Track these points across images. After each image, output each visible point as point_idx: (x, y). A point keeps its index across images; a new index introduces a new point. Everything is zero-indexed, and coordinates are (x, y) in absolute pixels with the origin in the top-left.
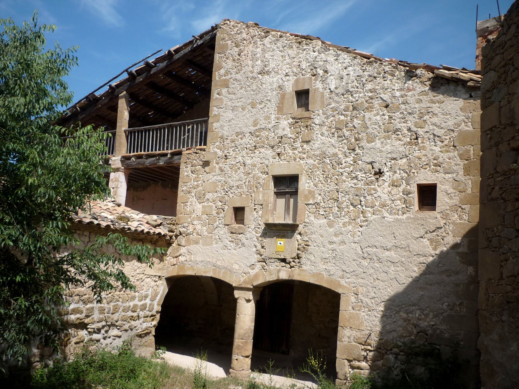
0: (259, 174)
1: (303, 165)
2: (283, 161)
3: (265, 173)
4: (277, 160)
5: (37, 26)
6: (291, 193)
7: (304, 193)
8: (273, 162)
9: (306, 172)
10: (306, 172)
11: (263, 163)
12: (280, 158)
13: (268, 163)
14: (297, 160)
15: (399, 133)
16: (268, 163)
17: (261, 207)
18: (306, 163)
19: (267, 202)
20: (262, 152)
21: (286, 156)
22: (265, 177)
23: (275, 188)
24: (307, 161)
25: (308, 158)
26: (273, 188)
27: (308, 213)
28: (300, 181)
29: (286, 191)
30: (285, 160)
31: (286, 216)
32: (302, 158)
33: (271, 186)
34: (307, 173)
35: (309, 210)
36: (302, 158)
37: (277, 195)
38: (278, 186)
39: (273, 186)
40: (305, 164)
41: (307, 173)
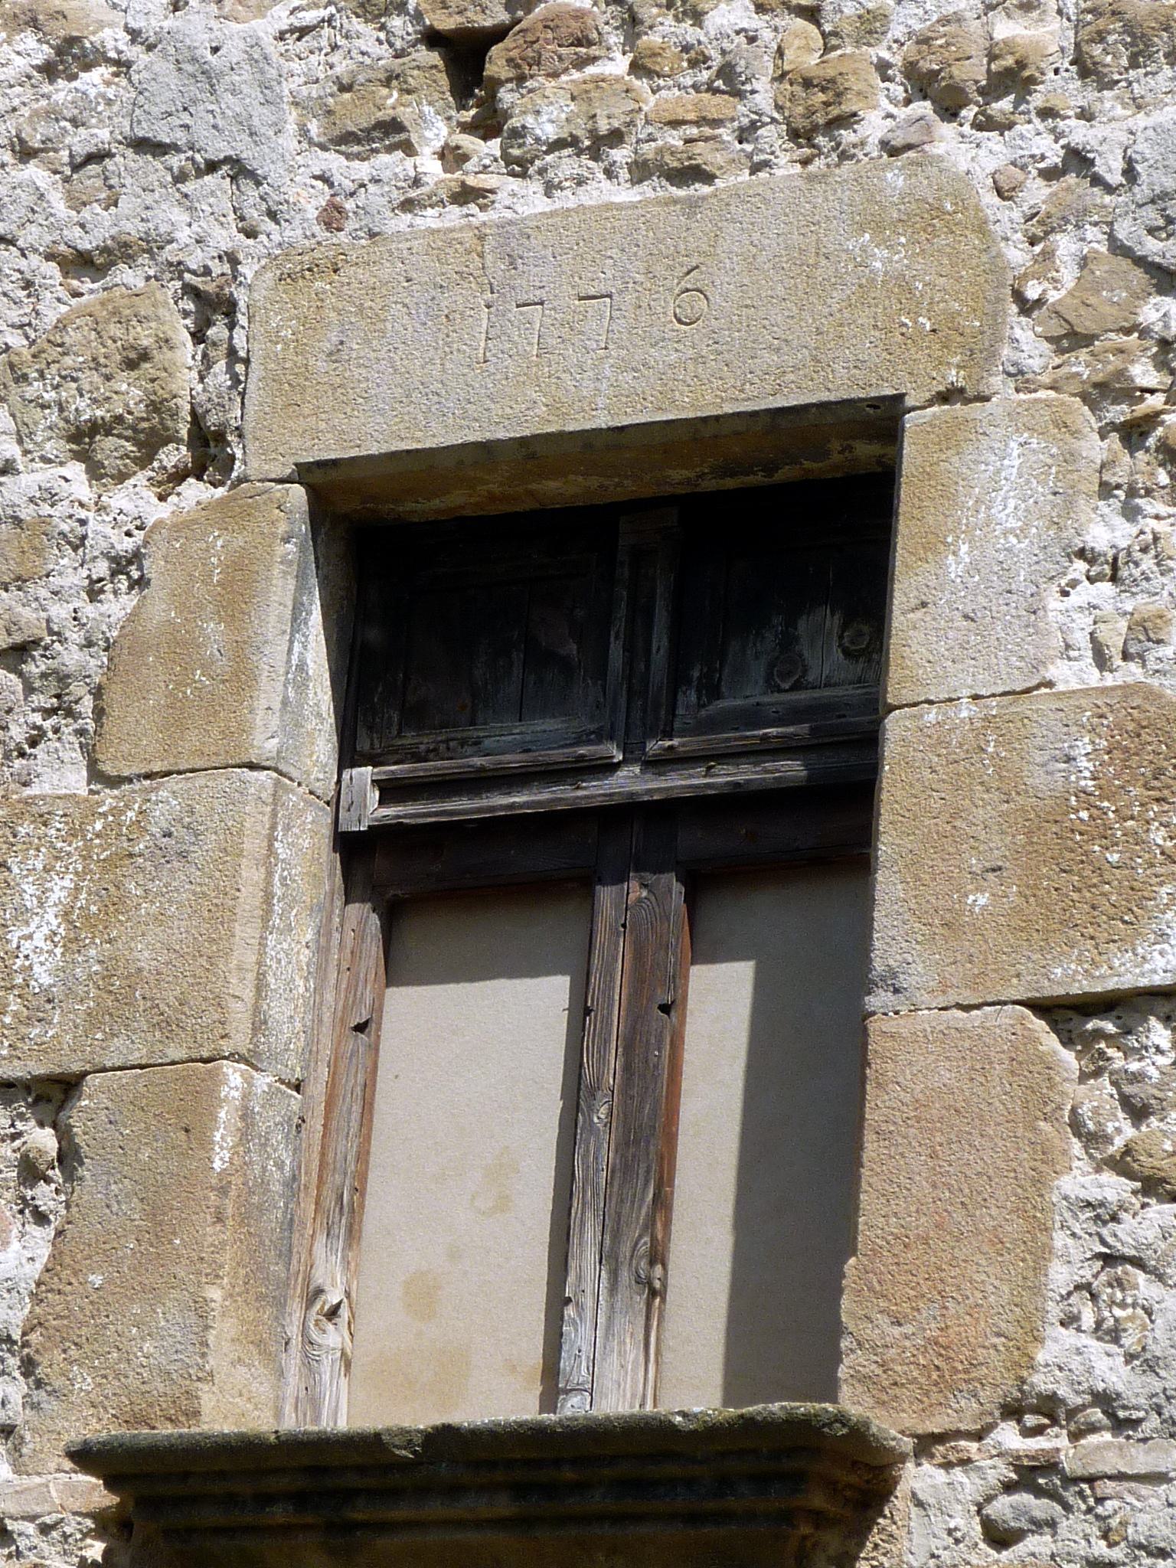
0: (30, 479)
1: (1006, 217)
2: (566, 165)
3: (149, 444)
4: (432, 168)
5: (1156, 521)
6: (692, 840)
7: (1009, 786)
8: (332, 217)
9: (1070, 340)
10: (1070, 340)
11: (121, 252)
12: (489, 124)
13: (225, 237)
14: (873, 127)
15: (704, 331)
16: (225, 237)
17: (45, 1140)
18: (1078, 160)
19: (166, 1026)
20: (112, 39)
21: (618, 65)
22: (158, 512)
23: (348, 756)
24: (1079, 134)
25: (1112, 58)
26: (324, 746)
27: (1114, 1188)
28: (935, 545)
29: (594, 790)
30: (600, 143)
31: (579, 1336)
32: (973, 72)
33: (269, 694)
34: (1081, 365)
35: (1123, 1131)
36: (973, 72)
37: (393, 917)
38: (416, 716)
39: (321, 696)
40: (1037, 193)
41: (1081, 365)
